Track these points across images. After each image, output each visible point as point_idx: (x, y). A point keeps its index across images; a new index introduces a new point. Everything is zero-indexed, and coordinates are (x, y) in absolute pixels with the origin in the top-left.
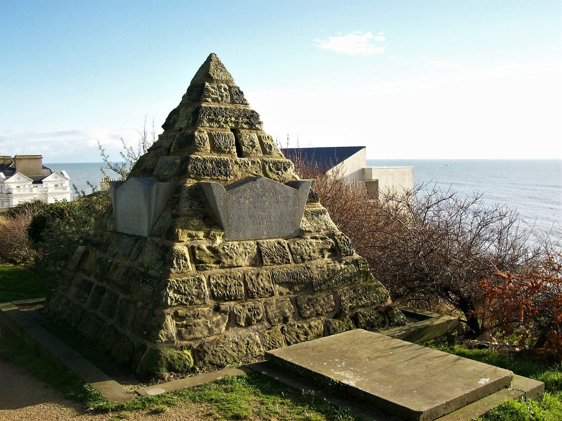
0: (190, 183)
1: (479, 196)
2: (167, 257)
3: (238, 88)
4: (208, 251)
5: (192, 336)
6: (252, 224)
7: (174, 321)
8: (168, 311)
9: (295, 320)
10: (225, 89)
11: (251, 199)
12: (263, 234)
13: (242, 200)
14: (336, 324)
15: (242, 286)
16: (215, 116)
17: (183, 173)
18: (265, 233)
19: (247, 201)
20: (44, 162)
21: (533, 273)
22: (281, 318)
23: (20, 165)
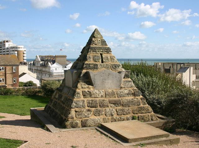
0: (84, 71)
2: (74, 93)
3: (104, 40)
4: (88, 92)
8: (72, 109)
10: (99, 41)
16: (94, 50)
17: (82, 68)
20: (67, 58)
21: (195, 97)
23: (57, 59)
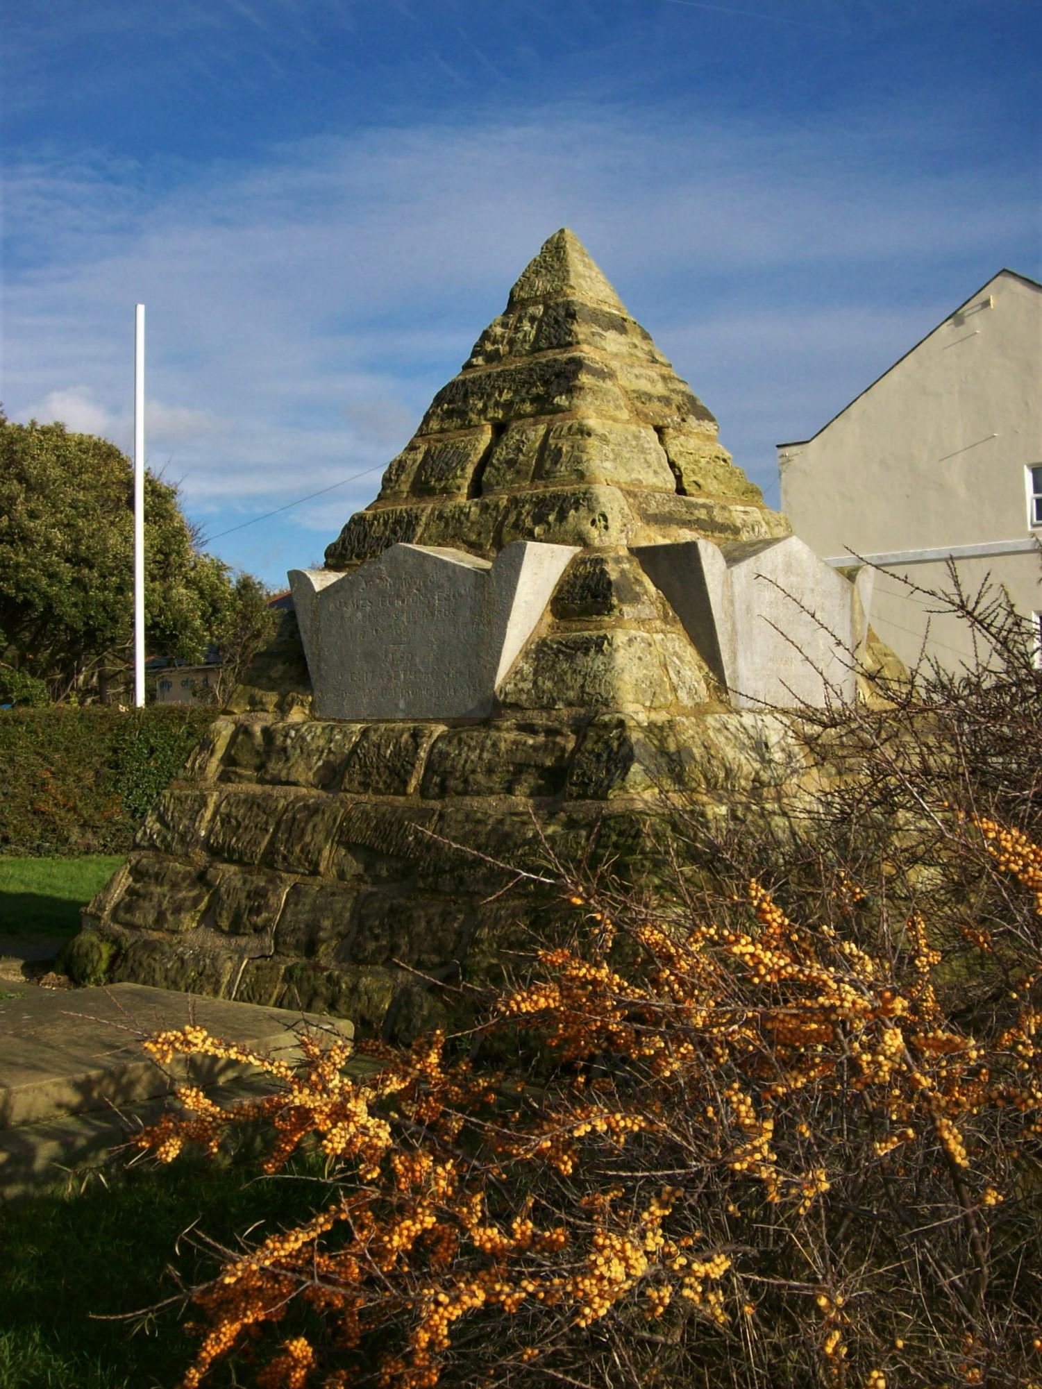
1: (957, 601)
5: (128, 917)
6: (370, 675)
7: (131, 879)
9: (337, 957)
11: (368, 608)
12: (397, 705)
13: (348, 611)
14: (421, 1007)
15: (267, 831)
18: (402, 704)
19: (359, 615)
22: (304, 938)
